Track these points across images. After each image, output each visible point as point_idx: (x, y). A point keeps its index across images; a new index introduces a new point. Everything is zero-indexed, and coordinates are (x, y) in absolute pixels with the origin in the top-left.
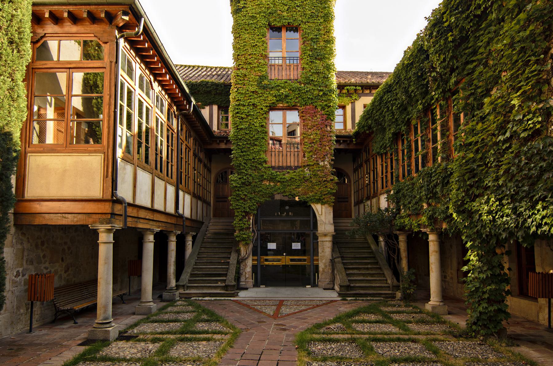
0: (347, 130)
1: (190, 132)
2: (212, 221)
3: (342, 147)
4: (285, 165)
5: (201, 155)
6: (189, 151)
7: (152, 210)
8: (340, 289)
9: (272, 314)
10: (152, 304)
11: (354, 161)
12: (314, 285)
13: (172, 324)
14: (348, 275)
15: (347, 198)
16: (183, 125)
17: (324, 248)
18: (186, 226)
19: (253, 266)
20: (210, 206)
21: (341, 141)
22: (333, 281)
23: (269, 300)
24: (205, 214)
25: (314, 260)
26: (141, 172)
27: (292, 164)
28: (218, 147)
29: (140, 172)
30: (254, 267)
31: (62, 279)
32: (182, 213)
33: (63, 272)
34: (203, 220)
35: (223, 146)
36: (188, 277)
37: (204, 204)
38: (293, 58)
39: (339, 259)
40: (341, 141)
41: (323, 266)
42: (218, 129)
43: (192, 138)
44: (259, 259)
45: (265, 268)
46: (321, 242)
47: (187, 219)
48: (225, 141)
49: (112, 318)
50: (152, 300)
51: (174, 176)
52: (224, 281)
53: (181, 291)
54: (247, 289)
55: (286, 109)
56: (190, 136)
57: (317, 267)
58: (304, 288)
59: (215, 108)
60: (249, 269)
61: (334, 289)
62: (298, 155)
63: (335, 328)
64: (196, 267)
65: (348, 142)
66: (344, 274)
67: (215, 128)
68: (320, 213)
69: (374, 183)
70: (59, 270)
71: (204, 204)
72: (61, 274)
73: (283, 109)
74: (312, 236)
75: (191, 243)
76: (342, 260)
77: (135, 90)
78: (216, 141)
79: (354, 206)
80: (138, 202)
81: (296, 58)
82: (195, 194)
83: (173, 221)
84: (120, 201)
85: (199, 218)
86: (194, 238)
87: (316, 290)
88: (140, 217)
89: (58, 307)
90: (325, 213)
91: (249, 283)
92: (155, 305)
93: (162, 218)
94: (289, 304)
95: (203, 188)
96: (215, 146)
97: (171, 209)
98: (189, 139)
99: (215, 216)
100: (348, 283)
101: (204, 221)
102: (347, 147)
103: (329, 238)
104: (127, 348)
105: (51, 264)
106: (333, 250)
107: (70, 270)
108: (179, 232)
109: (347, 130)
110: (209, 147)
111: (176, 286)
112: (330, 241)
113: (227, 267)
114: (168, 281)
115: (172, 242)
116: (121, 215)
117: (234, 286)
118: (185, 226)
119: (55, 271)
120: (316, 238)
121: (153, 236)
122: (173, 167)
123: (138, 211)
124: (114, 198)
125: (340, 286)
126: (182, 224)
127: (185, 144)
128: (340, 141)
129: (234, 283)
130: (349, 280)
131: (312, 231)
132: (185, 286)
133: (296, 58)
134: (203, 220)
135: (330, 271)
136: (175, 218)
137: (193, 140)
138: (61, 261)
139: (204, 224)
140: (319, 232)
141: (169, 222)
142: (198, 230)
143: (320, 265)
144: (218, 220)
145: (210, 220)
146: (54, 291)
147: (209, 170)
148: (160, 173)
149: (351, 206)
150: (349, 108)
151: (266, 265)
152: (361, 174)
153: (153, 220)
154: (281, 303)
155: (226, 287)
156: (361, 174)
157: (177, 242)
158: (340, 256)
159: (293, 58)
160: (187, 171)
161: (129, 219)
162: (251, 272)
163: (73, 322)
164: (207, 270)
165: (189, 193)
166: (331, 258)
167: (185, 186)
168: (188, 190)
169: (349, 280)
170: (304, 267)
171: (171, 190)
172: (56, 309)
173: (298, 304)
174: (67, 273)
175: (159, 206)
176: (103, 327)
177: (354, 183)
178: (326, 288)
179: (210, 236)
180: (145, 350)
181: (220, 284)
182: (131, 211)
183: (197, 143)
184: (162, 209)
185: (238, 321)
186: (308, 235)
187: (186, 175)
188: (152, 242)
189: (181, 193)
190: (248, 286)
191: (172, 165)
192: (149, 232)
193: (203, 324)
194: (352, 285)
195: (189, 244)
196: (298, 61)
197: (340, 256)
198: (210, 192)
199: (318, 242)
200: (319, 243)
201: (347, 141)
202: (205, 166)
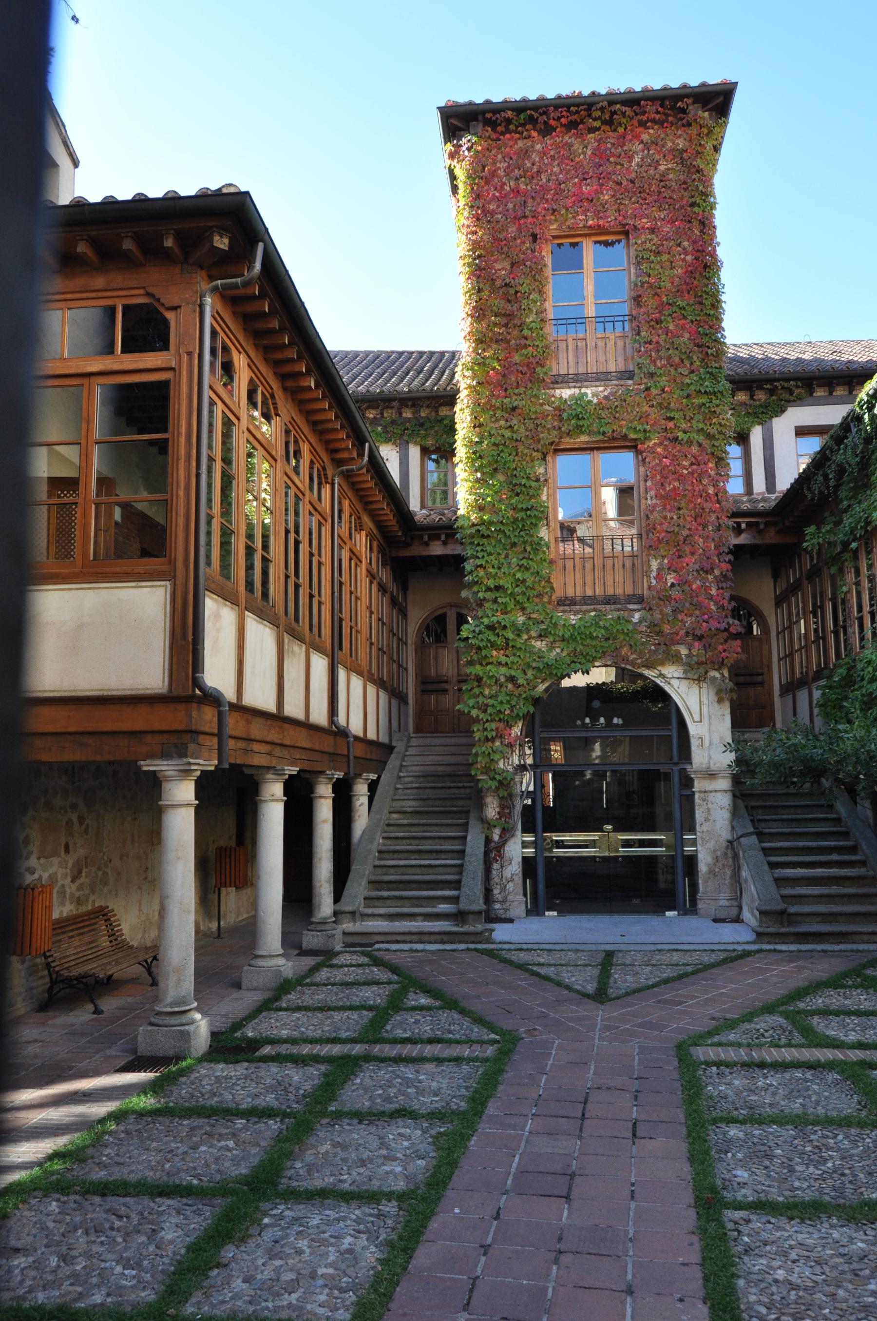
0: (755, 496)
1: (359, 518)
2: (414, 742)
3: (743, 539)
4: (599, 592)
5: (385, 575)
6: (356, 565)
7: (279, 719)
8: (761, 921)
9: (591, 988)
10: (282, 961)
11: (776, 577)
12: (691, 908)
13: (337, 1016)
14: (780, 882)
15: (762, 674)
16: (343, 500)
17: (709, 809)
18: (355, 757)
19: (526, 860)
20: (407, 703)
21: (743, 526)
22: (737, 899)
23: (577, 951)
24: (395, 726)
25: (535, 844)
26: (255, 623)
27: (619, 591)
28: (426, 553)
29: (252, 624)
30: (527, 862)
31: (65, 897)
32: (345, 725)
33: (69, 879)
34: (391, 740)
35: (437, 549)
36: (361, 888)
37: (393, 700)
38: (612, 319)
39: (754, 839)
40: (743, 526)
41: (709, 860)
42: (423, 507)
43: (363, 533)
44: (539, 841)
45: (556, 865)
46: (702, 795)
47: (356, 738)
48: (443, 537)
49: (196, 1000)
50: (281, 951)
51: (326, 631)
52: (456, 900)
53: (348, 926)
54: (511, 921)
55: (598, 449)
56: (360, 528)
57: (691, 862)
58: (660, 918)
59: (414, 452)
60: (514, 868)
61: (742, 921)
62: (633, 565)
63: (766, 1031)
64: (382, 863)
65: (762, 527)
66: (769, 878)
67: (414, 504)
68: (697, 718)
69: (836, 633)
70: (59, 875)
71: (393, 700)
72: (63, 886)
73: (592, 449)
74: (676, 779)
75: (364, 800)
76: (760, 842)
77: (239, 419)
78: (421, 537)
79: (782, 695)
80: (249, 700)
81: (621, 318)
82: (373, 675)
83: (327, 745)
84: (213, 698)
85: (384, 739)
86: (373, 787)
87: (691, 921)
88: (252, 737)
89: (57, 972)
90: (710, 717)
91: (516, 903)
92: (290, 964)
93: (302, 739)
94: (627, 962)
95: (391, 658)
96: (417, 550)
97: (319, 715)
98: (358, 536)
99: (418, 729)
100: (781, 906)
101: (394, 744)
102: (758, 541)
103: (724, 784)
104: (239, 1079)
105: (42, 861)
106: (735, 813)
107: (84, 874)
108: (293, 770)
109: (755, 496)
110: (404, 553)
111: (336, 914)
112: (726, 791)
113: (458, 862)
114: (315, 900)
115: (323, 800)
116: (231, 737)
117: (479, 913)
118: (351, 758)
119: (50, 876)
120: (687, 782)
121: (330, 787)
122: (323, 607)
123: (248, 722)
124: (197, 692)
125: (762, 913)
126: (345, 752)
127: (307, 500)
128: (739, 524)
129: (480, 905)
130: (783, 897)
131: (676, 764)
132: (357, 915)
133: (621, 318)
134: (391, 740)
135: (729, 872)
136: (331, 738)
137: (367, 536)
138: (63, 853)
139: (396, 750)
140: (695, 766)
141: (317, 747)
142: (380, 766)
143: (700, 856)
144: (428, 741)
145: (408, 741)
146: (51, 927)
147: (403, 613)
148: (294, 625)
149: (770, 693)
150: (756, 435)
151: (558, 858)
152: (797, 606)
153: (281, 745)
154: (608, 959)
155: (460, 916)
156: (797, 606)
157: (334, 800)
158: (752, 830)
159: (612, 319)
160: (354, 615)
161: (231, 744)
162: (521, 875)
163: (90, 1007)
164: (441, 870)
165: (360, 673)
166: (730, 838)
167: (351, 656)
168: (358, 664)
169: (783, 897)
170: (652, 860)
171: (320, 664)
172: (50, 975)
173: (653, 962)
174: (78, 883)
175: (293, 709)
176: (177, 1022)
177: (778, 633)
178: (718, 916)
179: (412, 782)
180: (282, 1086)
181: (443, 907)
182: (234, 724)
183: (375, 544)
184: (300, 715)
185: (507, 1008)
186: (667, 776)
187: (351, 628)
188: (282, 800)
189: (342, 674)
190: (512, 914)
191: (320, 603)
192: (270, 776)
193: (419, 1017)
194: (792, 910)
195: (362, 804)
196: (626, 324)
197: (752, 830)
198: (406, 669)
199: (693, 794)
200: (696, 796)
201: (757, 524)
202: (394, 602)
